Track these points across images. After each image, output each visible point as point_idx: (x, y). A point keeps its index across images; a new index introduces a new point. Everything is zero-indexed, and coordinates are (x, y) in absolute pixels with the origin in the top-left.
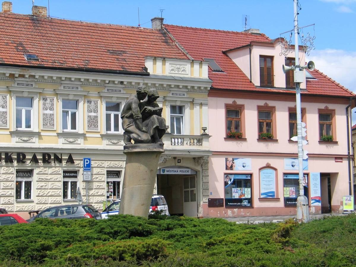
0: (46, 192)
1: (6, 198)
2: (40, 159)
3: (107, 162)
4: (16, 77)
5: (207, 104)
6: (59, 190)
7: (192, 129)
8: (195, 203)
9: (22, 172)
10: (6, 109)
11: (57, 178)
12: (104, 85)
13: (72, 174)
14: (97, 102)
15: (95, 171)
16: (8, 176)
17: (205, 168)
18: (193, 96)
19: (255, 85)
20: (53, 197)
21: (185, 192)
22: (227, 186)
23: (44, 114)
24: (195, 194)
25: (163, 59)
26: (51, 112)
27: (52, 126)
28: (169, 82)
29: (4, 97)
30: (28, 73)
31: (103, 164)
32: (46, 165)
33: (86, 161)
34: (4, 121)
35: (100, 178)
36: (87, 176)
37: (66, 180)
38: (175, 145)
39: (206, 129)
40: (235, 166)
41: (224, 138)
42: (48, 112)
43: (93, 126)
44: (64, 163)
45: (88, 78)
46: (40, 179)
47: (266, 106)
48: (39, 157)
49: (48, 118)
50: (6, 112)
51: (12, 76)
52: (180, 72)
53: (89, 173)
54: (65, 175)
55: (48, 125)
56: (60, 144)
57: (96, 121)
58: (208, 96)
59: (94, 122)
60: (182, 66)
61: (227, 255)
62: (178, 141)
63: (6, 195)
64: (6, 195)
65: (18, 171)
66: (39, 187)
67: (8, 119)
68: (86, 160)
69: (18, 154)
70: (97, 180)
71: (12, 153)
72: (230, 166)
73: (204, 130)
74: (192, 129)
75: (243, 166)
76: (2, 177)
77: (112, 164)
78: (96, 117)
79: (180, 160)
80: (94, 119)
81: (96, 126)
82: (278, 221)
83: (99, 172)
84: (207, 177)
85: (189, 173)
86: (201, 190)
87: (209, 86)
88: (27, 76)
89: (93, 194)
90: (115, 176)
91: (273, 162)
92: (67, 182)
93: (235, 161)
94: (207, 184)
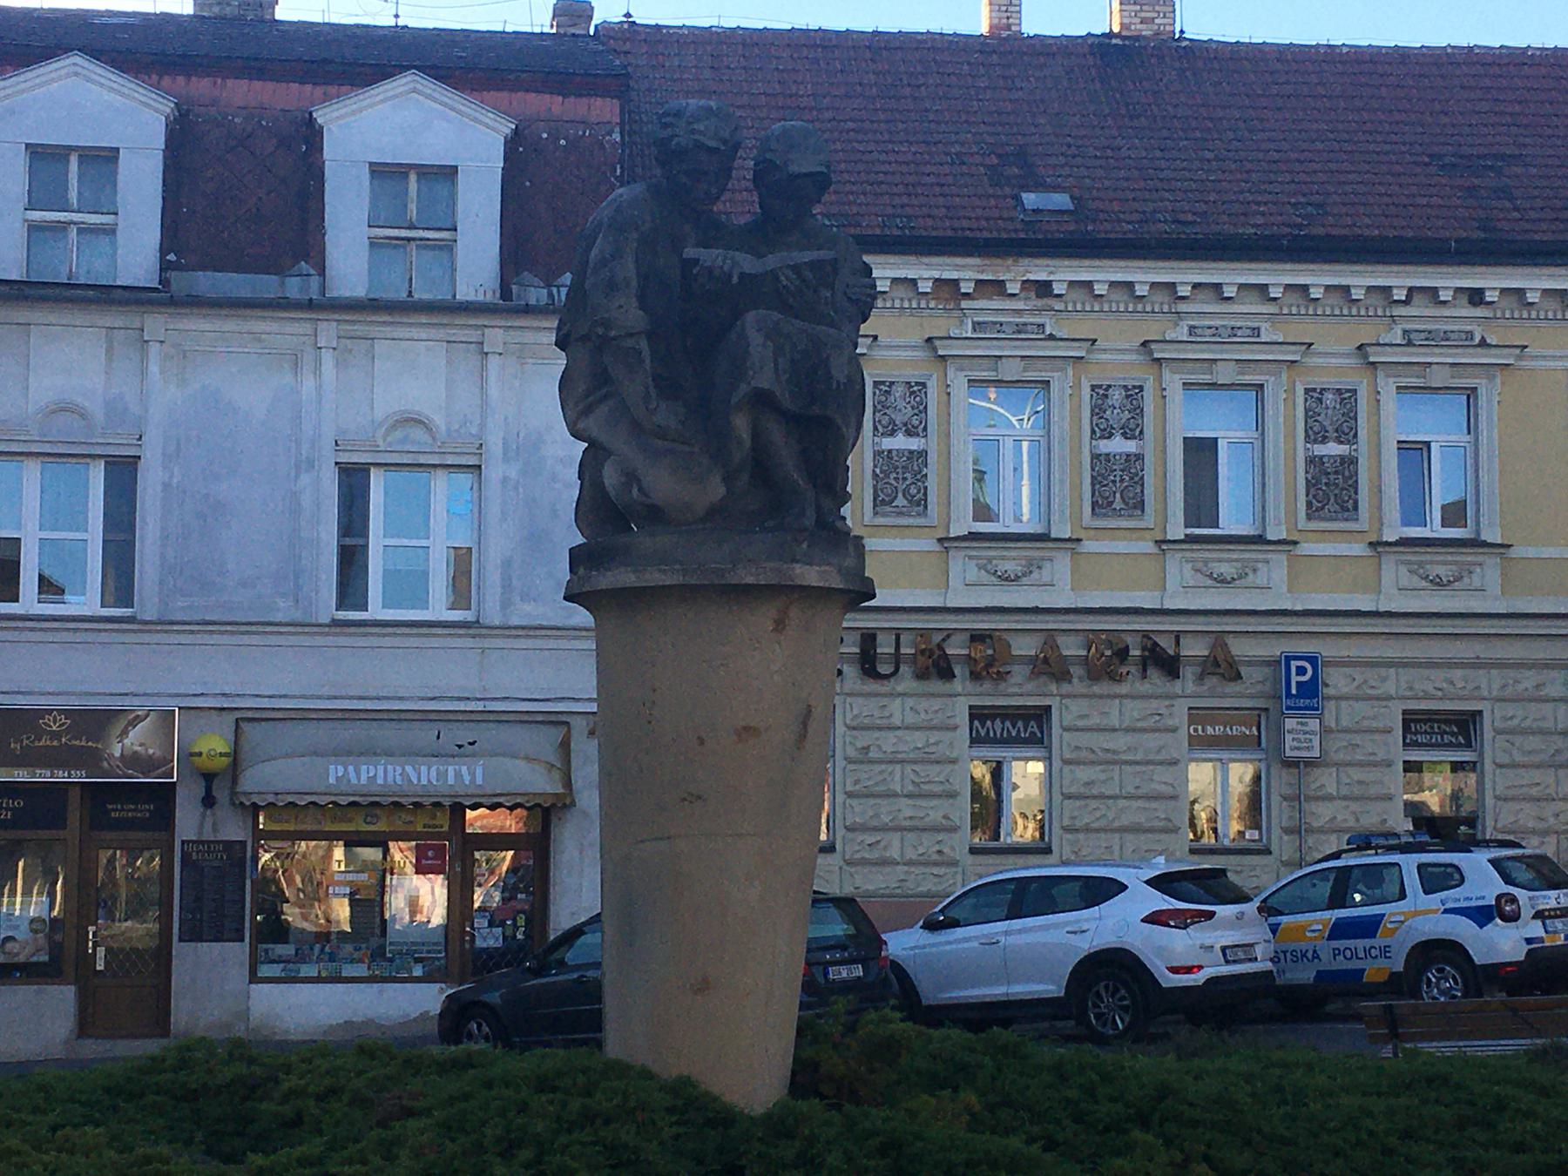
1: (925, 835)
4: (967, 296)
10: (923, 440)
26: (1131, 446)
27: (1135, 508)
30: (1017, 272)
33: (1298, 667)
34: (913, 491)
36: (1302, 737)
42: (1118, 445)
43: (1332, 506)
46: (1077, 748)
50: (923, 454)
53: (1314, 724)
54: (1200, 732)
55: (1118, 504)
65: (1195, 716)
67: (932, 484)
68: (1294, 664)
71: (949, 633)
78: (1350, 462)
81: (1350, 505)
88: (1013, 288)
90: (1453, 734)
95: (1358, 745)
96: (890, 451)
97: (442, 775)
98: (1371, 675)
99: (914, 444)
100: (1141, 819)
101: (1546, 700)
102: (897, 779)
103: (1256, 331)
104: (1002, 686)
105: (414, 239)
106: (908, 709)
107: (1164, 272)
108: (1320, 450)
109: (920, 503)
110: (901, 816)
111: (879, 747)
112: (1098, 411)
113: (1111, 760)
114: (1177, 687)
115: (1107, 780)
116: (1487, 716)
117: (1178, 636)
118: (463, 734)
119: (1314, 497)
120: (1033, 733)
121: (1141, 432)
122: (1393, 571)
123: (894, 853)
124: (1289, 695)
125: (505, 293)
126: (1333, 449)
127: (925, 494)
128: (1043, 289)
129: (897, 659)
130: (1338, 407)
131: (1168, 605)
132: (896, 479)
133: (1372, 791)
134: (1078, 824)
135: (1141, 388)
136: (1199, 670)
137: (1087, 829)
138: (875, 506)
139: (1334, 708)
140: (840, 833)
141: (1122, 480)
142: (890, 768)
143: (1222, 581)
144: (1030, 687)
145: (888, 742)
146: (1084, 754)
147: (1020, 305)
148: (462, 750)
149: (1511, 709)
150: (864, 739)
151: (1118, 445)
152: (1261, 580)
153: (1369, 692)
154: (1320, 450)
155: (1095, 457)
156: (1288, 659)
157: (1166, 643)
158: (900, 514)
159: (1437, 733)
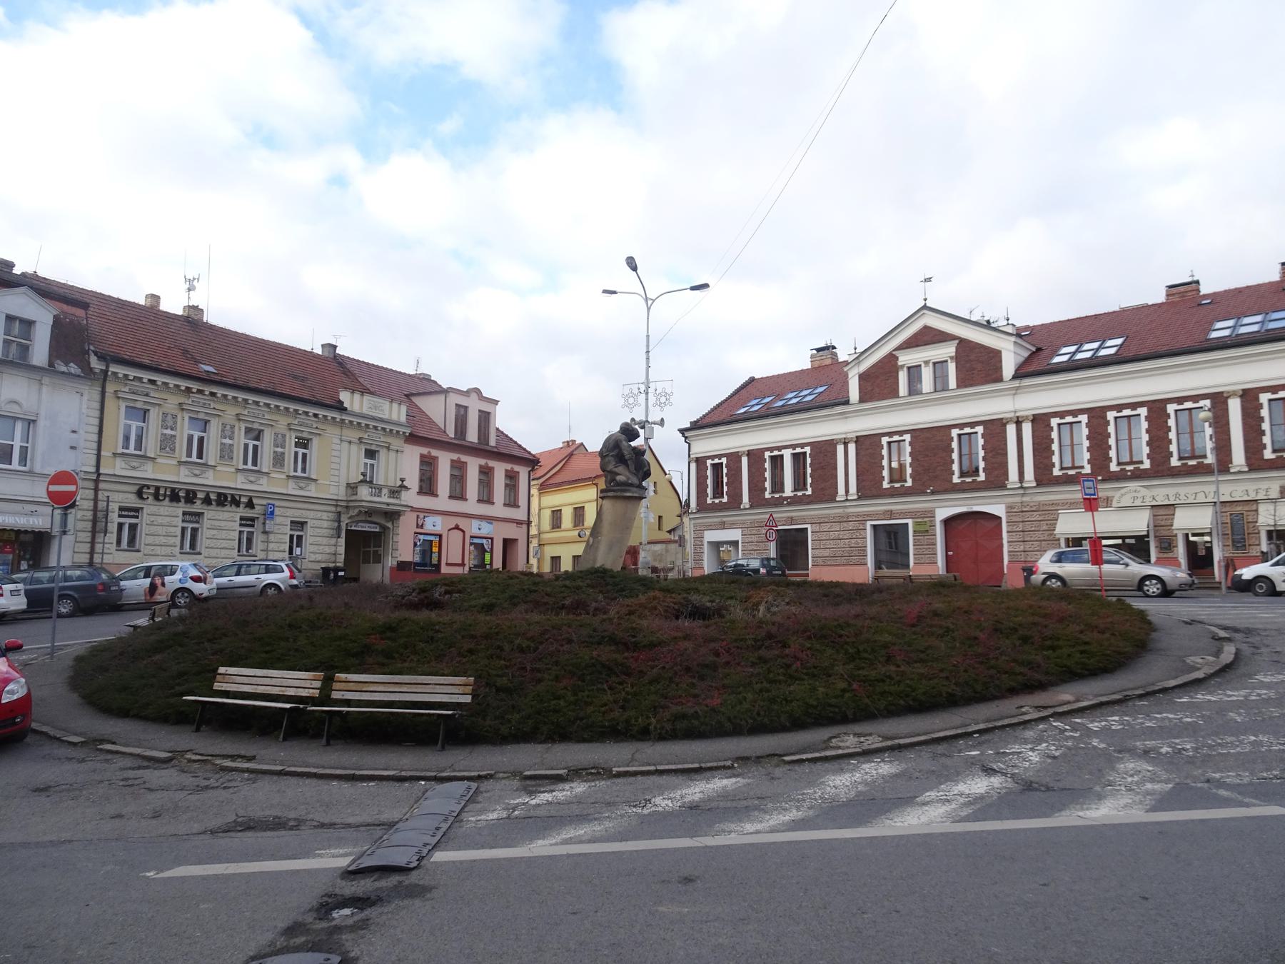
2: (183, 497)
7: (386, 479)
8: (381, 565)
13: (132, 514)
16: (173, 519)
18: (389, 440)
21: (364, 552)
23: (222, 444)
26: (231, 442)
30: (208, 389)
37: (185, 525)
42: (227, 441)
45: (236, 395)
47: (512, 470)
48: (213, 497)
51: (188, 390)
56: (239, 483)
61: (594, 615)
67: (177, 445)
69: (188, 491)
70: (280, 532)
71: (181, 489)
73: (403, 481)
74: (386, 479)
77: (297, 513)
78: (283, 453)
85: (377, 530)
91: (462, 523)
93: (426, 519)
97: (28, 521)
99: (173, 433)
100: (226, 546)
102: (161, 530)
103: (264, 415)
107: (139, 373)
112: (223, 431)
114: (238, 510)
116: (206, 514)
117: (240, 496)
118: (34, 508)
122: (291, 483)
123: (158, 553)
125: (51, 364)
126: (279, 450)
129: (165, 495)
131: (181, 481)
137: (212, 548)
139: (603, 548)
140: (143, 545)
143: (196, 475)
145: (160, 520)
148: (33, 513)
149: (315, 521)
150: (153, 518)
155: (222, 444)
157: (238, 498)
158: (168, 453)
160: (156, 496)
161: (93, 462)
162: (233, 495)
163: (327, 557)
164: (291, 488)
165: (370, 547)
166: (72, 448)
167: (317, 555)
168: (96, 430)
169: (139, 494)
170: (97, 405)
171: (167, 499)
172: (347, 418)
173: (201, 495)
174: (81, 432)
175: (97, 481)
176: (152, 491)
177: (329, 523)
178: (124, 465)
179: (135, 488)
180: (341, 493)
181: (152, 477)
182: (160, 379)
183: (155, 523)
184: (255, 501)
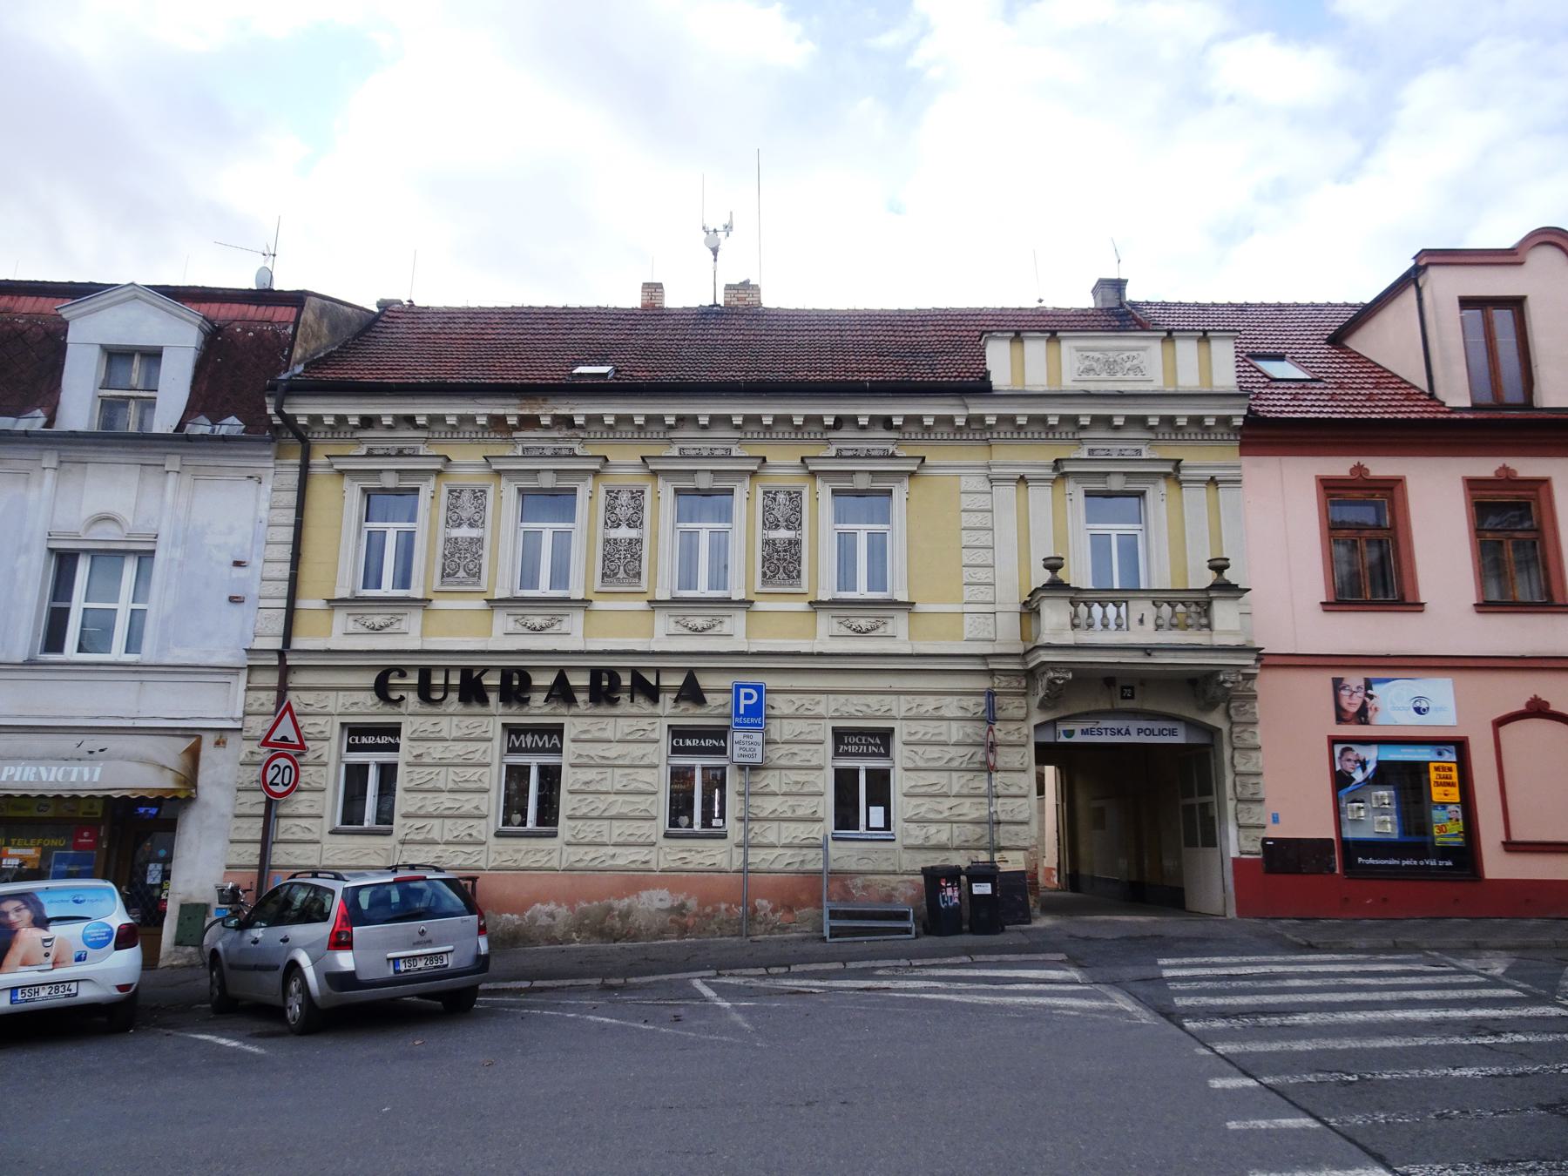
0: (601, 803)
1: (460, 821)
3: (835, 699)
4: (1084, 428)
5: (1239, 481)
6: (649, 797)
9: (866, 735)
10: (481, 530)
11: (644, 755)
12: (1074, 434)
13: (709, 743)
14: (800, 493)
15: (778, 729)
16: (472, 746)
17: (1243, 719)
19: (1447, 405)
20: (627, 823)
22: (1350, 788)
24: (1213, 817)
25: (1048, 335)
26: (633, 533)
27: (634, 576)
28: (1106, 406)
29: (479, 494)
30: (546, 411)
31: (818, 703)
32: (603, 710)
33: (745, 694)
34: (471, 566)
35: (804, 754)
36: (748, 747)
38: (1105, 626)
39: (1227, 567)
40: (1376, 709)
41: (1322, 603)
42: (624, 533)
43: (781, 575)
44: (667, 700)
46: (580, 756)
47: (1507, 480)
48: (579, 680)
49: (622, 553)
50: (480, 540)
52: (1119, 376)
53: (758, 737)
54: (357, 742)
55: (621, 574)
57: (795, 558)
58: (1241, 455)
59: (786, 560)
60: (1127, 354)
62: (1104, 613)
63: (463, 809)
64: (463, 809)
65: (676, 732)
66: (576, 787)
67: (485, 562)
68: (743, 691)
69: (507, 673)
70: (796, 762)
71: (486, 669)
72: (1354, 709)
75: (1418, 710)
76: (451, 751)
78: (796, 543)
79: (1132, 688)
80: (785, 551)
81: (794, 574)
82: (664, 939)
83: (801, 733)
84: (1254, 754)
85: (1180, 739)
86: (1231, 805)
87: (1238, 413)
88: (545, 421)
89: (777, 813)
90: (875, 745)
92: (364, 767)
93: (1377, 690)
94: (1254, 780)
95: (796, 754)
96: (456, 539)
97: (67, 774)
98: (806, 699)
100: (625, 810)
101: (942, 719)
102: (445, 778)
103: (1138, 451)
104: (526, 709)
105: (133, 398)
106: (454, 726)
108: (773, 534)
109: (476, 574)
110: (443, 807)
111: (429, 754)
113: (606, 765)
115: (602, 780)
117: (658, 671)
119: (768, 568)
120: (555, 745)
121: (641, 523)
123: (435, 835)
124: (738, 715)
126: (783, 534)
127: (480, 569)
128: (568, 421)
129: (447, 688)
130: (788, 503)
132: (459, 558)
133: (806, 790)
134: (578, 813)
135: (643, 492)
136: (674, 696)
137: (584, 817)
138: (443, 576)
139: (778, 726)
141: (625, 558)
142: (437, 770)
144: (547, 709)
146: (585, 760)
147: (555, 434)
150: (420, 748)
151: (624, 533)
152: (725, 629)
153: (807, 713)
154: (773, 534)
156: (738, 687)
159: (863, 745)
160: (425, 691)
161: (279, 627)
162: (635, 672)
163: (972, 832)
164: (826, 636)
165: (1191, 795)
166: (234, 600)
167: (933, 829)
168: (286, 552)
169: (382, 689)
170: (291, 498)
171: (454, 696)
172: (989, 411)
173: (545, 680)
174: (256, 562)
175: (285, 670)
176: (413, 679)
177: (970, 728)
178: (836, 628)
179: (370, 679)
180: (1005, 635)
181: (416, 646)
182: (422, 409)
183: (426, 760)
184: (705, 681)
